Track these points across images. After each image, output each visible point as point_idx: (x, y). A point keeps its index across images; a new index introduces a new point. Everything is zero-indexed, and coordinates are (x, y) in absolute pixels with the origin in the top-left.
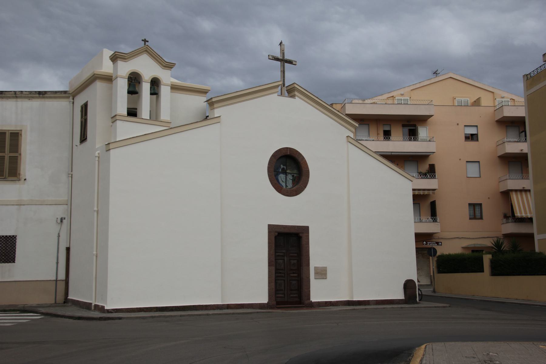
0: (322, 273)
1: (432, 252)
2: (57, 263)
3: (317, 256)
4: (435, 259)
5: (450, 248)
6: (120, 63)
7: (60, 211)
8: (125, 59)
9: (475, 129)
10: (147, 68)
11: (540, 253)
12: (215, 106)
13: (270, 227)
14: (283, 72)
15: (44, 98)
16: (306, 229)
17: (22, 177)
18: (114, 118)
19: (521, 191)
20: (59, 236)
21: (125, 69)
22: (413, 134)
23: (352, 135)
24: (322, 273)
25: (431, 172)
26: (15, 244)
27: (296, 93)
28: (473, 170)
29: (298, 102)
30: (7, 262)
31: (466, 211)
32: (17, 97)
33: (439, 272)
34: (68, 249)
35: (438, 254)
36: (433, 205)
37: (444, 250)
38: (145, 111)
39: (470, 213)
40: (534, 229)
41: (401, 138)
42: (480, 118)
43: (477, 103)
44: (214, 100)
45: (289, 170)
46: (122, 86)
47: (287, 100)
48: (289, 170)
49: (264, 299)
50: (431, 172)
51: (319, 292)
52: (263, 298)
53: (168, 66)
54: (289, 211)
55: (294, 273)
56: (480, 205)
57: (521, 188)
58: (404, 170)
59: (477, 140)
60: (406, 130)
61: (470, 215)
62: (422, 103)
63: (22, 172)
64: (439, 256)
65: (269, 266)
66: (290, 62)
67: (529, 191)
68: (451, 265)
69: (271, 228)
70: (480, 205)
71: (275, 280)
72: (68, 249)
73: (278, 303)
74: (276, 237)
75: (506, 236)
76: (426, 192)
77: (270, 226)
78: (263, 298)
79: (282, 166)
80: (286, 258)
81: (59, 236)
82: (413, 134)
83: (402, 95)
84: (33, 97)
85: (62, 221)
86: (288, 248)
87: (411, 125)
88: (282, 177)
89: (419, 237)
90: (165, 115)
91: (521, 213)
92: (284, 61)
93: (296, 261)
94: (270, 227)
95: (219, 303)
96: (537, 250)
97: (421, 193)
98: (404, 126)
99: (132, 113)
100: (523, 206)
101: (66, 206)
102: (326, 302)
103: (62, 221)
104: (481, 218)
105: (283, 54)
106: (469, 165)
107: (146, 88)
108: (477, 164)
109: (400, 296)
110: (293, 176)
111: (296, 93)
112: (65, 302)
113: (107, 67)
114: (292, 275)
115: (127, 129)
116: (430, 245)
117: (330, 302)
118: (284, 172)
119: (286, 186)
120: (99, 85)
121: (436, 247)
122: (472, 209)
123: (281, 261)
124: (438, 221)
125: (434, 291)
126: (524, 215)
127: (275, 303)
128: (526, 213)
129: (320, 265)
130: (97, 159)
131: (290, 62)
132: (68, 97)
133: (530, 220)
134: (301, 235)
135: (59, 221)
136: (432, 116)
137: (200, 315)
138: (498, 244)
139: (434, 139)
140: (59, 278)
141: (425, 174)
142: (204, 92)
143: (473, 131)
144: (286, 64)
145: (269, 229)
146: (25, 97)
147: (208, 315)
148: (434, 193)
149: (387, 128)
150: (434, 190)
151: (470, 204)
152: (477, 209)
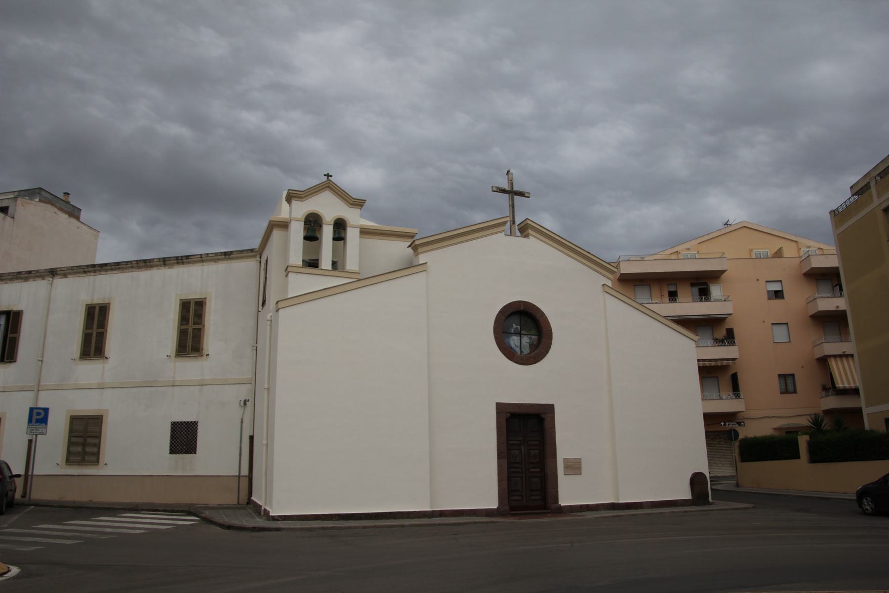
0: (574, 467)
1: (732, 435)
2: (240, 455)
3: (566, 444)
4: (737, 444)
5: (757, 428)
6: (295, 203)
7: (243, 392)
8: (301, 198)
9: (779, 284)
10: (329, 208)
11: (872, 431)
12: (420, 250)
13: (499, 406)
14: (513, 206)
15: (230, 259)
16: (550, 408)
17: (205, 352)
18: (287, 271)
19: (841, 356)
20: (242, 422)
21: (301, 209)
22: (704, 295)
23: (609, 283)
24: (574, 467)
25: (729, 338)
26: (98, 437)
27: (530, 231)
28: (780, 334)
29: (533, 243)
30: (188, 453)
31: (776, 383)
32: (203, 261)
33: (744, 460)
34: (252, 438)
35: (741, 437)
36: (734, 378)
37: (751, 431)
38: (326, 262)
39: (780, 386)
40: (862, 402)
41: (690, 299)
42: (784, 272)
43: (778, 254)
44: (417, 243)
45: (524, 329)
46: (297, 230)
47: (518, 241)
48: (524, 329)
49: (494, 504)
50: (729, 338)
51: (570, 492)
52: (492, 502)
53: (358, 203)
54: (525, 385)
55: (535, 468)
56: (793, 375)
57: (841, 353)
58: (696, 338)
59: (783, 298)
60: (696, 290)
61: (781, 389)
62: (712, 256)
63: (205, 347)
64: (742, 440)
65: (499, 458)
66: (521, 194)
67: (852, 356)
68: (758, 450)
69: (501, 408)
70: (793, 375)
71: (509, 478)
72: (252, 438)
73: (512, 508)
74: (508, 420)
75: (827, 412)
76: (725, 363)
77: (498, 405)
78: (492, 502)
79: (515, 326)
80: (523, 447)
81: (242, 422)
82: (704, 295)
83: (688, 249)
84: (219, 260)
85: (245, 404)
86: (526, 435)
87: (702, 283)
88: (514, 341)
89: (708, 418)
90: (352, 263)
91: (849, 383)
92: (513, 193)
93: (537, 452)
94: (499, 406)
95: (427, 508)
96: (867, 426)
97: (719, 363)
98: (692, 285)
99: (312, 264)
100: (846, 375)
101: (249, 386)
102: (581, 506)
103: (245, 404)
104: (795, 392)
105: (512, 184)
106: (775, 327)
107: (327, 232)
108: (785, 327)
109: (686, 495)
110: (530, 338)
111: (530, 231)
112: (248, 503)
113: (284, 211)
114: (532, 470)
115: (303, 283)
116: (730, 425)
117: (588, 505)
118: (520, 334)
119: (521, 352)
120: (276, 234)
121: (738, 429)
122: (783, 381)
123: (517, 452)
124: (742, 396)
125: (738, 485)
126: (846, 385)
127: (507, 508)
128: (849, 383)
129: (571, 456)
130: (269, 323)
131: (521, 194)
132: (255, 256)
133: (855, 392)
134: (543, 416)
135: (242, 404)
136: (725, 271)
137: (391, 526)
138: (817, 422)
139: (730, 298)
140: (242, 474)
141: (722, 341)
142: (410, 236)
143: (776, 287)
144: (516, 197)
145: (497, 409)
146: (211, 260)
147: (403, 526)
148: (734, 363)
149: (672, 289)
150: (734, 359)
151: (779, 375)
152: (789, 381)
